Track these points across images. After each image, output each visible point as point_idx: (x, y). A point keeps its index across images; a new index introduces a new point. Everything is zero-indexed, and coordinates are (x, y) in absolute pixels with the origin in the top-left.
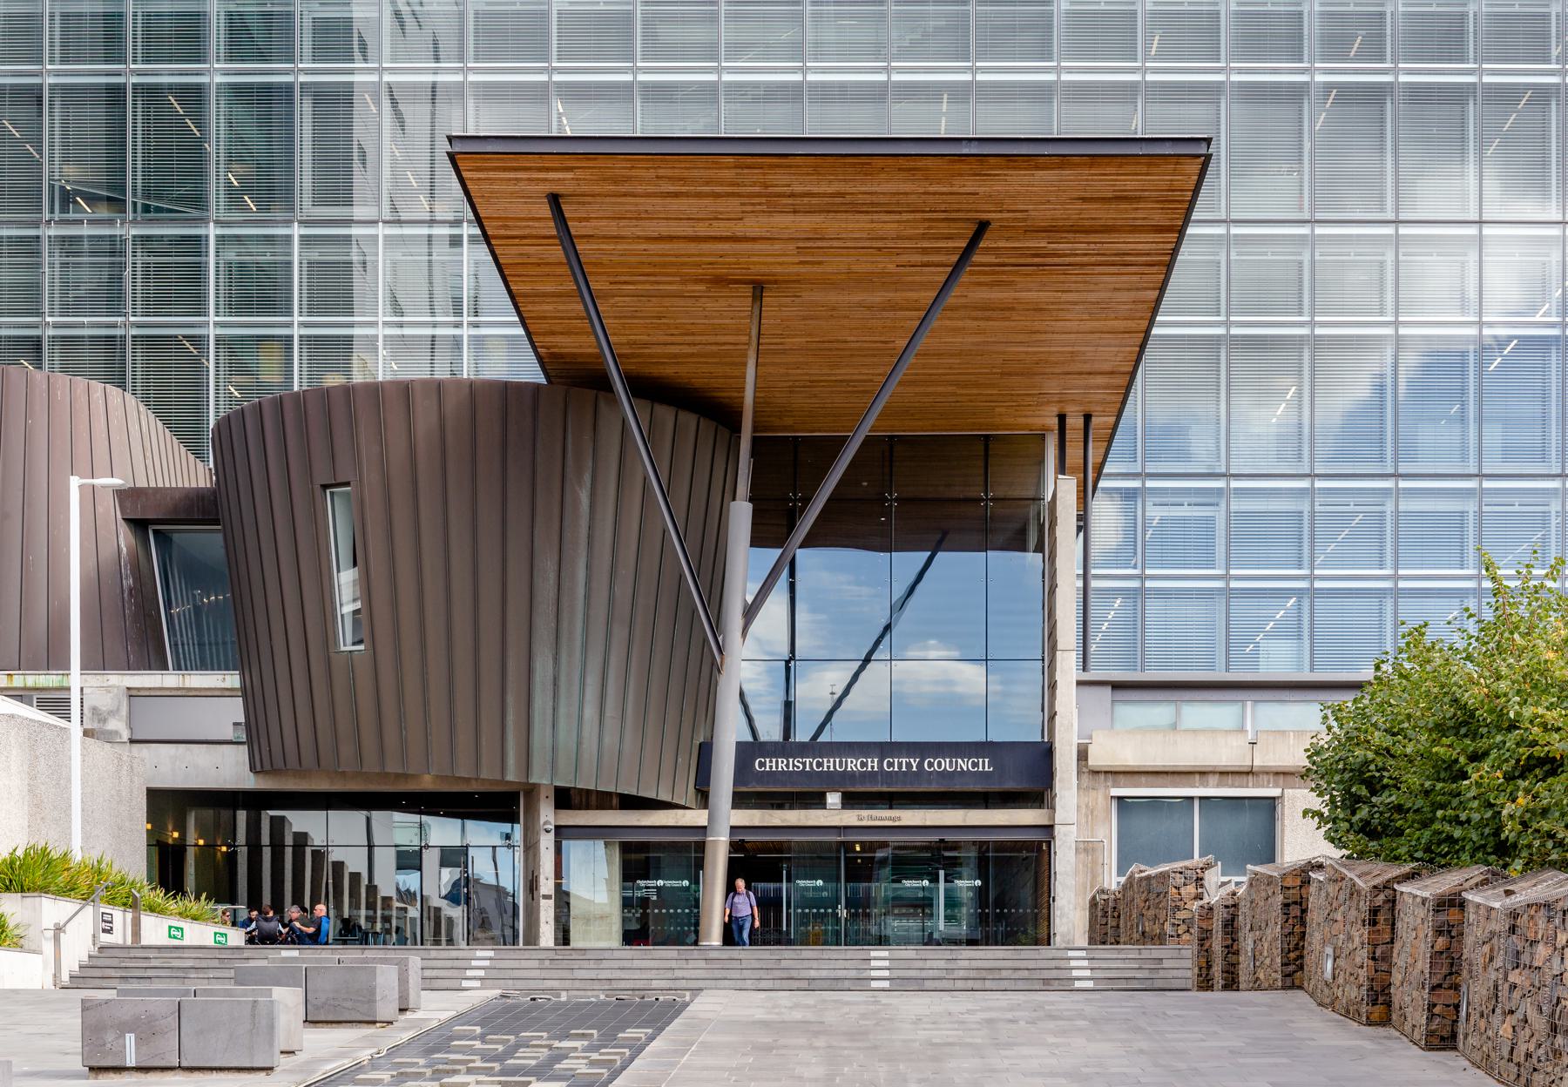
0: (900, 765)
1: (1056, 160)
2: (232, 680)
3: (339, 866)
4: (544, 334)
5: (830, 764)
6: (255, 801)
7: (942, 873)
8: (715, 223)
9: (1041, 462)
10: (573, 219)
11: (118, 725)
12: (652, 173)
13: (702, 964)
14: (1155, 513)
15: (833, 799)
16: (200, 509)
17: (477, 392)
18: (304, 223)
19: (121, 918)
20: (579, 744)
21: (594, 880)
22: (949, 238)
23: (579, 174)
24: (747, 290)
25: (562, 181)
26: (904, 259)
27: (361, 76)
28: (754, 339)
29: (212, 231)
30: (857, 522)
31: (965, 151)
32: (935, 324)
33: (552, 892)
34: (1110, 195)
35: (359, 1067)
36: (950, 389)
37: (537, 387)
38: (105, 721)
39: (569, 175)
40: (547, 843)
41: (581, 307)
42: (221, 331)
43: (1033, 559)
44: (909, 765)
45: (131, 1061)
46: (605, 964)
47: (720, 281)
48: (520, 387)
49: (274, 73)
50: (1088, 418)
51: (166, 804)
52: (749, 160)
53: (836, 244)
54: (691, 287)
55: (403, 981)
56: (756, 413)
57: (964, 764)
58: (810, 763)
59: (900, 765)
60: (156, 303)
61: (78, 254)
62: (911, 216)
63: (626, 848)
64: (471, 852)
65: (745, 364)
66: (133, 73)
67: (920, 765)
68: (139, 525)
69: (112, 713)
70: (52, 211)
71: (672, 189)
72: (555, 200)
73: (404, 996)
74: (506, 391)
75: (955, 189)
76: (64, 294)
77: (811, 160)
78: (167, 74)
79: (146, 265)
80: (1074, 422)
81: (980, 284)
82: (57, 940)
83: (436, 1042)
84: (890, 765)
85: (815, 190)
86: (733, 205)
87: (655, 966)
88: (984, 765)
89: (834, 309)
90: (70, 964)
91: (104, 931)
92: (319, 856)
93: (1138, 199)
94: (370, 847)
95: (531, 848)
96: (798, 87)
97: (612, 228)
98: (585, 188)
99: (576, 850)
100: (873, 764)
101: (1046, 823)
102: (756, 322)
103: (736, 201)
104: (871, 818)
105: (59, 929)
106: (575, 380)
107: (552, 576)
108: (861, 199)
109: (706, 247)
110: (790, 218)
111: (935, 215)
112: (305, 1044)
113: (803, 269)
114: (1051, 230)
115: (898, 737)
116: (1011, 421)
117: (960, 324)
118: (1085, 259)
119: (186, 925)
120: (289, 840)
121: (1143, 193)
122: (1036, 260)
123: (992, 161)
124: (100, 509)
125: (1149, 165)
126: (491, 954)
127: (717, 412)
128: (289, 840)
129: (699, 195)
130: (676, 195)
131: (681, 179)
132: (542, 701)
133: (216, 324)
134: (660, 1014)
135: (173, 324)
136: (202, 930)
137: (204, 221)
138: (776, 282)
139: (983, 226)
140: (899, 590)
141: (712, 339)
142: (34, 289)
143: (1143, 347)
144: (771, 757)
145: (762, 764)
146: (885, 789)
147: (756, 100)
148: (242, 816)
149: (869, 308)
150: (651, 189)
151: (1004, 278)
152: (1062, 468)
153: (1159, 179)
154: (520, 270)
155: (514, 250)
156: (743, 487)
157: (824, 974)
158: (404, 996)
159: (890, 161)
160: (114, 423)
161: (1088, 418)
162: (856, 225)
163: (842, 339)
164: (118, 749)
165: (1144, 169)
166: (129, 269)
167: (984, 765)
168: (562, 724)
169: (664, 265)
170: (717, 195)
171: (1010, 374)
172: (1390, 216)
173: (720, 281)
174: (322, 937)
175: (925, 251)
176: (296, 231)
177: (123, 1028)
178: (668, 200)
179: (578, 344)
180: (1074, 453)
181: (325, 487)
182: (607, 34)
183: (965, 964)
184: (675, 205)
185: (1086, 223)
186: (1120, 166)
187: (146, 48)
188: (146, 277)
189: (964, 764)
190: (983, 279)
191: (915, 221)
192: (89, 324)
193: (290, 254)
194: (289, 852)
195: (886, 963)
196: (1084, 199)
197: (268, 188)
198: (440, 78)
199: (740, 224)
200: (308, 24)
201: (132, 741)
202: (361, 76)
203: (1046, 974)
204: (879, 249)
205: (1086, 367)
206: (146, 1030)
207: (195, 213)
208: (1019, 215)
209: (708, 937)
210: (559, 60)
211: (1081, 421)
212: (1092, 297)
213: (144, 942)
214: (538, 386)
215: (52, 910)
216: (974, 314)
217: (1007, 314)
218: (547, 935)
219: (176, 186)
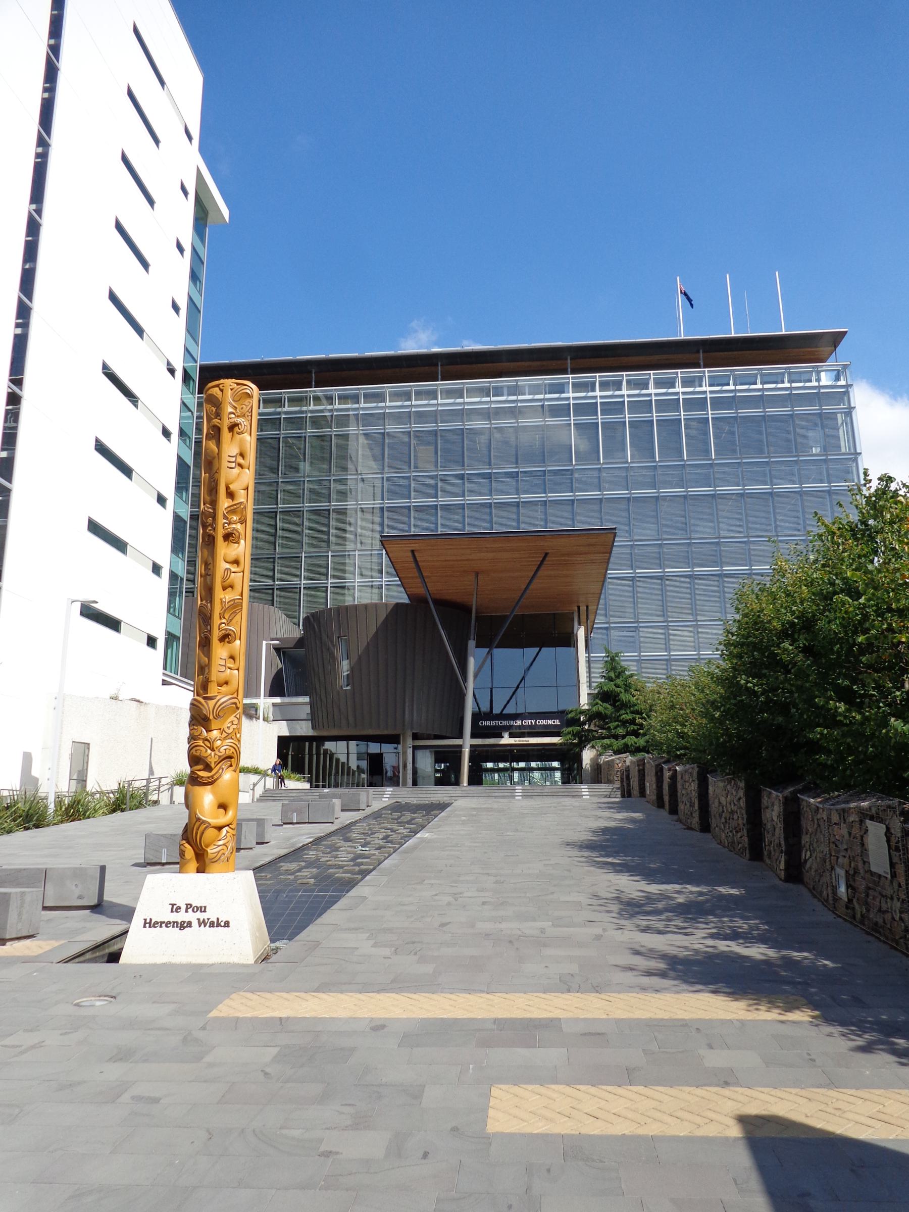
2: (306, 699)
9: (573, 620)
15: (506, 735)
27: (350, 504)
30: (514, 640)
37: (407, 605)
48: (402, 604)
49: (323, 505)
50: (587, 607)
51: (283, 742)
55: (368, 797)
56: (476, 609)
58: (498, 723)
72: (413, 551)
73: (368, 802)
80: (583, 608)
82: (253, 789)
83: (377, 815)
87: (442, 793)
90: (257, 796)
92: (332, 755)
94: (348, 754)
95: (405, 753)
99: (419, 754)
121: (600, 543)
134: (442, 807)
136: (296, 784)
139: (546, 554)
143: (604, 582)
148: (307, 744)
152: (580, 624)
158: (368, 802)
161: (587, 607)
179: (421, 591)
189: (550, 722)
206: (299, 812)
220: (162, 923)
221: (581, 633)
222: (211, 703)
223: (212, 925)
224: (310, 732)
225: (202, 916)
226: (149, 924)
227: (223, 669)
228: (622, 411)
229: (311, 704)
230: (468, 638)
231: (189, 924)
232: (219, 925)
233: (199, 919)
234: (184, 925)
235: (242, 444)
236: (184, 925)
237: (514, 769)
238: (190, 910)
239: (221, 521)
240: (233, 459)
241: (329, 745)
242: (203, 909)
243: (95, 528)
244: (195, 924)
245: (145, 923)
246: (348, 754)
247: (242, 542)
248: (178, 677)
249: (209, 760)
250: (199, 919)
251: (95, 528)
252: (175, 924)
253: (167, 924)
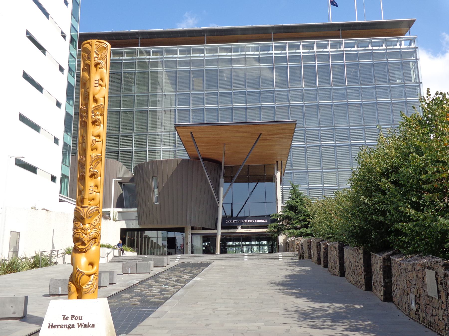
2: (136, 209)
14: (295, 176)
15: (240, 228)
21: (198, 242)
25: (192, 130)
27: (159, 108)
30: (243, 179)
32: (254, 148)
35: (134, 286)
43: (274, 183)
50: (282, 161)
51: (123, 232)
55: (168, 260)
63: (203, 237)
64: (176, 238)
72: (191, 132)
73: (168, 262)
80: (279, 162)
83: (172, 269)
90: (109, 259)
92: (149, 238)
94: (157, 237)
95: (187, 237)
99: (194, 237)
106: (194, 159)
120: (144, 237)
121: (288, 129)
127: (218, 163)
128: (144, 237)
136: (130, 253)
139: (261, 134)
140: (251, 191)
143: (290, 148)
148: (140, 232)
152: (277, 170)
156: (222, 176)
158: (168, 262)
161: (282, 161)
172: (334, 125)
177: (128, 267)
179: (195, 153)
187: (124, 105)
189: (262, 221)
194: (144, 239)
197: (144, 127)
202: (159, 108)
206: (132, 268)
220: (58, 325)
221: (278, 175)
222: (85, 210)
223: (85, 326)
224: (138, 227)
225: (80, 322)
226: (51, 326)
227: (92, 192)
228: (299, 61)
229: (138, 211)
231: (73, 326)
232: (89, 326)
233: (78, 324)
234: (70, 327)
235: (101, 74)
236: (70, 327)
237: (243, 245)
238: (74, 319)
239: (90, 114)
240: (97, 82)
242: (80, 318)
243: (22, 118)
244: (76, 326)
245: (49, 326)
246: (157, 237)
247: (102, 125)
248: (68, 197)
249: (84, 239)
250: (78, 324)
251: (22, 118)
252: (65, 326)
253: (61, 326)
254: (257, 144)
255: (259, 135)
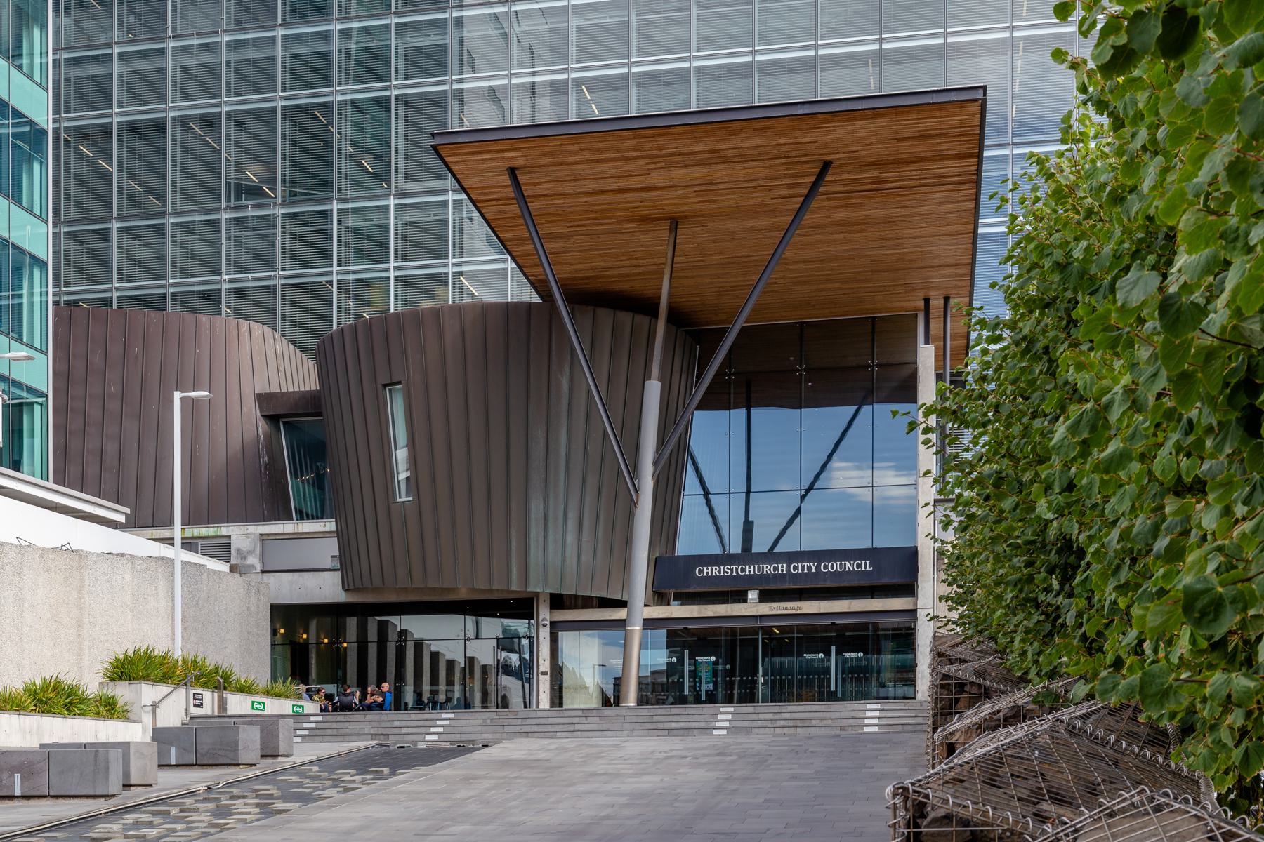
0: (803, 568)
1: (869, 112)
2: (329, 525)
3: (435, 656)
4: (531, 266)
5: (751, 569)
6: (362, 611)
7: (833, 648)
8: (631, 179)
10: (506, 186)
11: (254, 561)
12: (576, 147)
13: (597, 720)
15: (753, 595)
16: (311, 405)
17: (486, 310)
18: (397, 196)
19: (209, 696)
20: (563, 561)
22: (804, 175)
23: (526, 152)
24: (666, 225)
25: (516, 157)
26: (776, 193)
28: (669, 260)
29: (335, 206)
31: (800, 112)
33: (548, 670)
34: (917, 134)
36: (837, 285)
38: (245, 558)
39: (519, 154)
40: (545, 634)
41: (531, 247)
42: (340, 277)
44: (809, 568)
45: (18, 792)
46: (529, 721)
47: (645, 220)
50: (947, 299)
51: (288, 617)
52: (643, 132)
53: (722, 186)
54: (625, 226)
57: (851, 566)
59: (803, 568)
60: (298, 260)
61: (245, 229)
62: (772, 162)
65: (662, 278)
66: (398, 87)
67: (818, 568)
68: (273, 419)
69: (250, 552)
70: (228, 200)
71: (593, 157)
72: (512, 171)
74: (509, 310)
75: (799, 140)
76: (238, 257)
77: (688, 128)
78: (305, 97)
79: (293, 235)
80: (937, 302)
81: (836, 207)
82: (154, 712)
84: (795, 568)
85: (696, 149)
86: (640, 165)
88: (866, 566)
89: (733, 233)
91: (195, 706)
92: (419, 645)
93: (939, 136)
96: (749, 65)
97: (558, 188)
98: (532, 162)
99: (566, 638)
100: (782, 568)
101: (911, 607)
102: (671, 248)
103: (641, 162)
104: (779, 609)
105: (154, 706)
107: (542, 441)
108: (731, 153)
109: (629, 196)
110: (684, 170)
111: (789, 160)
112: (159, 780)
113: (703, 206)
114: (879, 164)
115: (805, 548)
116: (888, 305)
117: (830, 237)
118: (911, 183)
119: (268, 701)
122: (874, 186)
123: (821, 117)
124: (245, 410)
125: (940, 110)
126: (452, 716)
129: (614, 160)
130: (598, 161)
131: (598, 150)
132: (535, 532)
133: (338, 273)
135: (308, 274)
137: (329, 200)
138: (686, 217)
139: (827, 165)
141: (652, 261)
142: (216, 256)
143: (974, 243)
144: (750, 564)
145: (701, 572)
146: (792, 586)
147: (720, 78)
149: (760, 230)
150: (578, 158)
151: (854, 201)
152: (927, 342)
153: (950, 120)
154: (502, 223)
155: (494, 209)
157: (682, 725)
159: (745, 124)
160: (255, 348)
161: (947, 299)
162: (735, 172)
163: (741, 258)
164: (254, 578)
165: (938, 114)
166: (279, 238)
167: (866, 566)
168: (551, 547)
169: (602, 211)
170: (627, 159)
171: (879, 271)
173: (645, 220)
174: (386, 706)
175: (789, 186)
176: (392, 202)
178: (593, 165)
180: (935, 327)
181: (385, 386)
182: (599, 42)
183: (787, 716)
184: (600, 169)
185: (904, 156)
186: (918, 112)
187: (293, 80)
188: (293, 243)
189: (851, 566)
190: (838, 203)
191: (775, 165)
192: (251, 279)
193: (388, 218)
195: (877, 714)
196: (898, 139)
198: (537, 79)
199: (649, 178)
200: (401, 53)
201: (263, 572)
203: (845, 722)
204: (755, 187)
205: (936, 262)
207: (324, 194)
208: (852, 155)
209: (626, 700)
210: (698, 50)
211: (942, 302)
212: (925, 209)
213: (229, 713)
214: (530, 305)
215: (149, 692)
216: (840, 229)
217: (864, 227)
218: (545, 701)
219: (312, 177)
221: (926, 357)
229: (339, 534)
230: (646, 376)
241: (419, 627)
248: (50, 485)
254: (809, 218)
255: (816, 169)
